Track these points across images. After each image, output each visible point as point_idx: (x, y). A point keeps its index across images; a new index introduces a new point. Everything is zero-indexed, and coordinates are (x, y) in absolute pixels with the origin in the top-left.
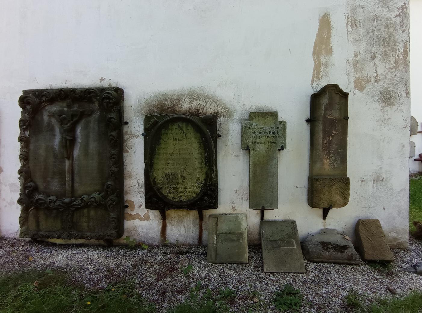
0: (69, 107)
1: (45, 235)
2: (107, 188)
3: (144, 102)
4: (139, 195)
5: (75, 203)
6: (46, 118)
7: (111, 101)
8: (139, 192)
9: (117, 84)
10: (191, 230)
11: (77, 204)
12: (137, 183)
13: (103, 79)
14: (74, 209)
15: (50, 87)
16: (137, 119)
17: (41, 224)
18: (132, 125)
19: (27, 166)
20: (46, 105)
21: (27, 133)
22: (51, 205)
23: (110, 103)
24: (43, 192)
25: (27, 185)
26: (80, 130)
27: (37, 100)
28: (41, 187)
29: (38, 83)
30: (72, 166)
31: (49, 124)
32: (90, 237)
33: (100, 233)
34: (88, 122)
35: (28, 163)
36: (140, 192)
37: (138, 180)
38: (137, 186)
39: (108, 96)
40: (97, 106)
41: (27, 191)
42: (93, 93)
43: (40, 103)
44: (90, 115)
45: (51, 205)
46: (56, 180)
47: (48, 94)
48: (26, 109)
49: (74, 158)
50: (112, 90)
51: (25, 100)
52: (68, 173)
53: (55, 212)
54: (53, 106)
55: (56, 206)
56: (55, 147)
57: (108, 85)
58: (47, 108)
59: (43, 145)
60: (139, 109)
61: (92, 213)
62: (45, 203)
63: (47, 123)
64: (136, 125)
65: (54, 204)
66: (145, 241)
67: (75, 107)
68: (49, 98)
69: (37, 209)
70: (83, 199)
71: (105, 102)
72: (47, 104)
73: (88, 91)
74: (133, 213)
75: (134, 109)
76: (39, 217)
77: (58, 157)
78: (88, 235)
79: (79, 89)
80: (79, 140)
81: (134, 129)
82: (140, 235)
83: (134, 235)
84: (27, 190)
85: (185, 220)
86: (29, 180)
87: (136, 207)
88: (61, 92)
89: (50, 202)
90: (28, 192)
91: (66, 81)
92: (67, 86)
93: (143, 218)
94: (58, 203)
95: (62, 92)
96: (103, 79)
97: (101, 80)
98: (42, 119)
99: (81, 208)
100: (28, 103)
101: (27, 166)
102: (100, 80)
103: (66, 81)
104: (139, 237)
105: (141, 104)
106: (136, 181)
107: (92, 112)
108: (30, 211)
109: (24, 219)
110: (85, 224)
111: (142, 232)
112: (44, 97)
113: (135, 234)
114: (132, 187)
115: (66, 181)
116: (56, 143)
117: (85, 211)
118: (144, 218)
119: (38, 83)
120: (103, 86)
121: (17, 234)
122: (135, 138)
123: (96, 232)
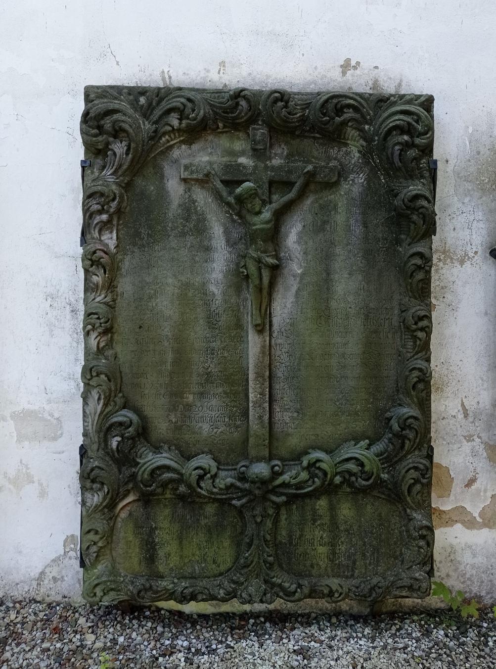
0: (258, 153)
1: (180, 590)
2: (403, 429)
3: (488, 148)
4: (467, 447)
5: (286, 477)
6: (174, 187)
7: (418, 141)
8: (465, 437)
9: (400, 85)
11: (293, 482)
12: (460, 408)
13: (353, 63)
14: (284, 498)
15: (164, 79)
16: (463, 203)
17: (161, 553)
18: (448, 221)
20: (172, 143)
21: (110, 240)
22: (201, 488)
23: (412, 145)
24: (165, 443)
25: (115, 419)
26: (300, 235)
27: (147, 126)
28: (161, 427)
29: (118, 63)
30: (268, 351)
31: (189, 209)
32: (341, 594)
33: (375, 581)
34: (327, 209)
35: (110, 344)
36: (469, 438)
37: (464, 400)
38: (461, 416)
39: (409, 124)
40: (357, 155)
41: (114, 443)
42: (351, 110)
43: (155, 136)
44: (331, 186)
45: (201, 488)
46: (214, 402)
47: (189, 105)
49: (276, 327)
51: (107, 123)
52: (259, 375)
53: (210, 509)
54: (195, 147)
55: (221, 489)
56: (213, 288)
57: (370, 83)
58: (176, 153)
59: (170, 281)
60: (472, 169)
61: (346, 511)
62: (181, 480)
63: (180, 205)
64: (460, 220)
65: (213, 482)
66: (483, 593)
67: (276, 154)
68: (195, 119)
69: (147, 500)
70: (317, 465)
71: (398, 143)
72: (175, 141)
73: (335, 101)
74: (446, 506)
75: (454, 171)
76: (156, 528)
77: (220, 323)
78: (334, 589)
79: (298, 94)
80: (295, 267)
81: (453, 234)
82: (468, 576)
83: (448, 575)
84: (114, 437)
86: (119, 401)
87: (457, 487)
88: (239, 99)
89: (201, 478)
90: (119, 442)
91: (223, 64)
92: (224, 82)
93: (478, 519)
94: (226, 478)
95: (243, 103)
96: (353, 63)
97: (346, 66)
98: (162, 193)
99: (309, 495)
100: (117, 133)
101: (109, 353)
102: (341, 66)
103: (220, 65)
104: (463, 583)
105: (478, 153)
106: (458, 402)
107: (342, 173)
108: (122, 509)
109: (101, 538)
110: (322, 550)
111: (473, 566)
112: (172, 114)
113: (450, 573)
114: (444, 422)
116: (214, 276)
117: (322, 504)
118: (481, 521)
119: (118, 63)
120: (350, 88)
121: (39, 584)
122: (457, 264)
123: (356, 575)
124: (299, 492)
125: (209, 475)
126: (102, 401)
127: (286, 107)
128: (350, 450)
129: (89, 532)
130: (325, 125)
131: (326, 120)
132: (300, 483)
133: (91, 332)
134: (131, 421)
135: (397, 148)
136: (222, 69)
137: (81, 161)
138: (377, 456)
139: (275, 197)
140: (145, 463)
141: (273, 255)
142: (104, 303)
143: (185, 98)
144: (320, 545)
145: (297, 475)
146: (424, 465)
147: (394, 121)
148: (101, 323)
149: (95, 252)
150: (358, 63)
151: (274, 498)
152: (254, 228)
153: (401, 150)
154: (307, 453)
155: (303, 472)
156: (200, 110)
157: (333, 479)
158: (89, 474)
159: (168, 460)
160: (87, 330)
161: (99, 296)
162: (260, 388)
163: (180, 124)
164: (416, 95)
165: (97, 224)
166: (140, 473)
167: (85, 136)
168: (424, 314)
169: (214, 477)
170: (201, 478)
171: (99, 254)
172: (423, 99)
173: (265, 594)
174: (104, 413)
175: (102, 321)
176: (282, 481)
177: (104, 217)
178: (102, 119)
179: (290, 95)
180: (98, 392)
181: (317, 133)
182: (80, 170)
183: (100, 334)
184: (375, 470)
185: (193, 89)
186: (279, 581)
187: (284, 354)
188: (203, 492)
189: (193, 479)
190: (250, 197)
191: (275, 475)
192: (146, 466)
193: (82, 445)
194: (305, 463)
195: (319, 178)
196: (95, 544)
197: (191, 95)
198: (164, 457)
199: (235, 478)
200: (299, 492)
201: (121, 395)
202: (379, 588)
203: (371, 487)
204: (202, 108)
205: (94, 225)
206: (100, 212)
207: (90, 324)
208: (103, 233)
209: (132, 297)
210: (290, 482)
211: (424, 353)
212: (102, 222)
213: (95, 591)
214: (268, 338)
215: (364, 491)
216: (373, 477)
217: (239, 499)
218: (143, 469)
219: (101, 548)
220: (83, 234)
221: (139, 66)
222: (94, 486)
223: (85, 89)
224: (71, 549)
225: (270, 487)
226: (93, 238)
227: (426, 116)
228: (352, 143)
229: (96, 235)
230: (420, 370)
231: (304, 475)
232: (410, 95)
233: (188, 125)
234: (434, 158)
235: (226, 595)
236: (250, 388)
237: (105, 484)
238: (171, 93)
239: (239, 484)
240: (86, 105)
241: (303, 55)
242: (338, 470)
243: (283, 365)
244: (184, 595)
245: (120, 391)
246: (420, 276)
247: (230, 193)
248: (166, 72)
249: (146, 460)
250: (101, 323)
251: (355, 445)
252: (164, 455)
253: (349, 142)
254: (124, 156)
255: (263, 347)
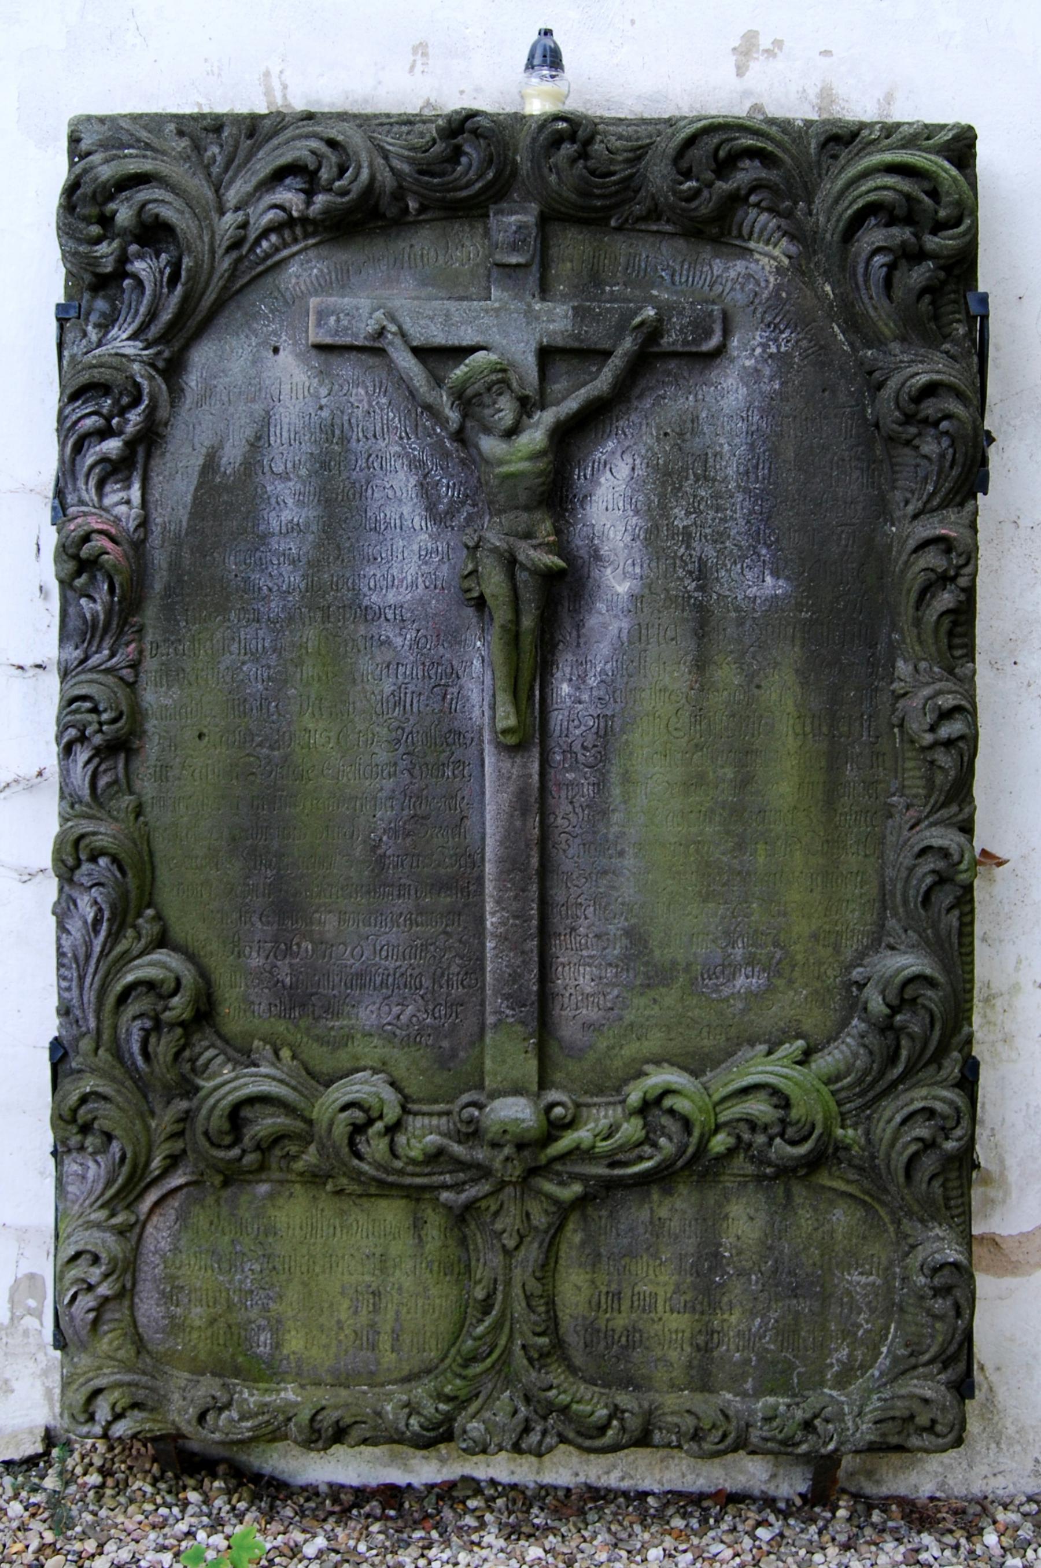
2: (895, 1010)
5: (583, 1135)
7: (932, 242)
9: (889, 98)
10: (433, 1291)
11: (603, 1146)
13: (765, 42)
15: (268, 92)
19: (127, 801)
20: (285, 253)
22: (359, 1156)
39: (908, 197)
45: (359, 1156)
47: (333, 158)
48: (127, 282)
50: (927, 150)
51: (124, 214)
52: (511, 864)
55: (413, 1161)
57: (812, 93)
68: (344, 193)
70: (667, 1102)
85: (473, 1226)
86: (148, 928)
89: (358, 1129)
96: (765, 42)
115: (490, 945)
124: (618, 1172)
125: (379, 1125)
126: (105, 926)
127: (583, 154)
128: (755, 1065)
129: (77, 1255)
130: (689, 199)
131: (690, 188)
132: (621, 1148)
133: (77, 748)
134: (178, 981)
135: (879, 260)
136: (419, 63)
137: (58, 306)
138: (826, 1084)
139: (557, 387)
140: (216, 1088)
141: (548, 544)
142: (108, 671)
143: (321, 139)
144: (672, 1311)
145: (611, 1132)
146: (951, 1103)
147: (877, 189)
148: (101, 724)
149: (86, 538)
150: (778, 43)
151: (549, 1187)
152: (498, 470)
153: (892, 267)
154: (641, 1074)
155: (628, 1121)
156: (359, 167)
157: (708, 1141)
158: (74, 1111)
159: (274, 1083)
160: (65, 740)
161: (96, 652)
162: (516, 897)
163: (309, 203)
164: (926, 126)
165: (92, 467)
166: (204, 1112)
167: (72, 245)
168: (956, 702)
169: (393, 1129)
170: (358, 1129)
171: (100, 542)
172: (946, 136)
173: (527, 1430)
174: (111, 957)
175: (105, 717)
176: (574, 1145)
177: (112, 446)
178: (111, 198)
179: (596, 125)
180: (96, 902)
181: (668, 221)
182: (54, 325)
183: (98, 752)
184: (819, 1118)
185: (342, 117)
186: (564, 1399)
187: (578, 810)
188: (365, 1167)
189: (341, 1130)
190: (489, 389)
191: (555, 1128)
192: (217, 1095)
193: (56, 1039)
194: (634, 1098)
195: (669, 341)
196: (90, 1288)
197: (333, 132)
198: (266, 1076)
199: (446, 1135)
200: (618, 1172)
201: (150, 912)
202: (827, 1421)
203: (815, 1163)
204: (365, 164)
205: (85, 469)
206: (104, 433)
207: (73, 726)
208: (108, 488)
209: (150, 664)
210: (594, 1147)
211: (954, 808)
212: (104, 460)
213: (91, 1409)
214: (536, 767)
215: (786, 1172)
216: (814, 1136)
217: (457, 1187)
218: (212, 1101)
219: (106, 1299)
220: (59, 493)
221: (206, 60)
222: (89, 1141)
223: (70, 125)
224: (30, 1312)
225: (543, 1159)
226: (82, 502)
227: (954, 179)
228: (761, 246)
229: (90, 494)
230: (944, 853)
231: (632, 1129)
232: (910, 124)
233: (327, 212)
234: (981, 289)
235: (428, 1430)
236: (488, 899)
237: (116, 1137)
238: (285, 128)
239: (457, 1149)
240: (72, 164)
241: (633, 22)
242: (723, 1118)
243: (578, 840)
244: (317, 1426)
245: (149, 905)
246: (946, 599)
247: (438, 382)
248: (275, 71)
249: (219, 1080)
250: (101, 724)
251: (770, 1053)
252: (263, 1070)
253: (752, 245)
254: (165, 290)
255: (522, 793)
